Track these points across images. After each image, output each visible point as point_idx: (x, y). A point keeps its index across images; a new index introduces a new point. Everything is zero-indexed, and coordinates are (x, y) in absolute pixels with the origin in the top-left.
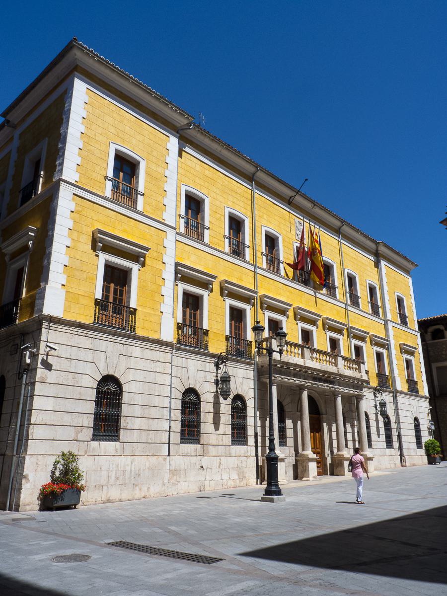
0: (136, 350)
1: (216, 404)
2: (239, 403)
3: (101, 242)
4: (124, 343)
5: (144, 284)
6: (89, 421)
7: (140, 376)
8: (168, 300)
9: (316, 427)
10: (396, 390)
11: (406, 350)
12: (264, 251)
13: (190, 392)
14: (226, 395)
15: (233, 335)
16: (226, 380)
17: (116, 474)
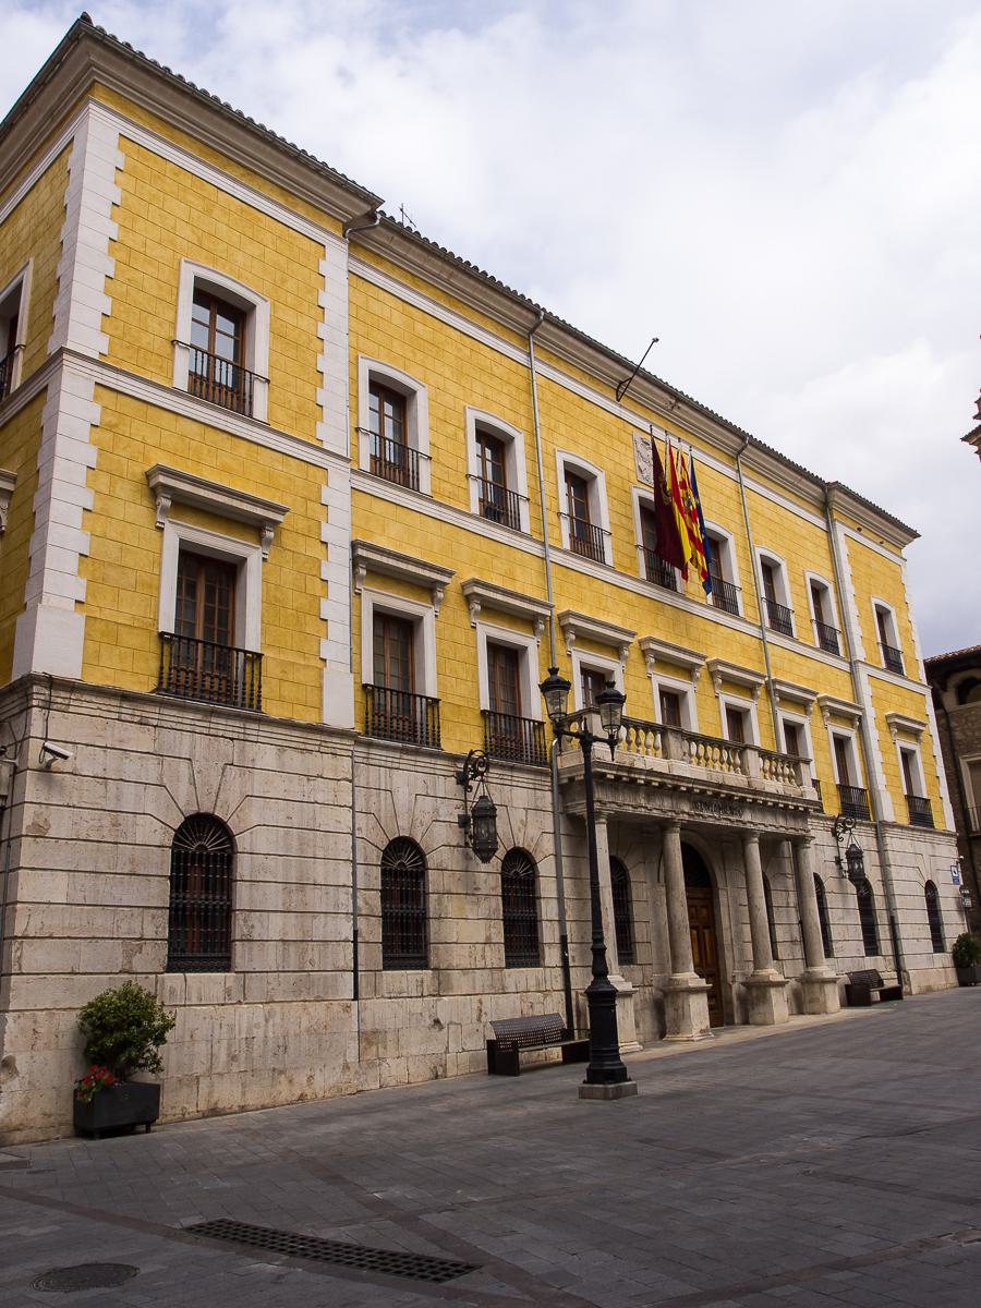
5: (279, 595)
8: (339, 631)
14: (485, 850)
17: (229, 1047)
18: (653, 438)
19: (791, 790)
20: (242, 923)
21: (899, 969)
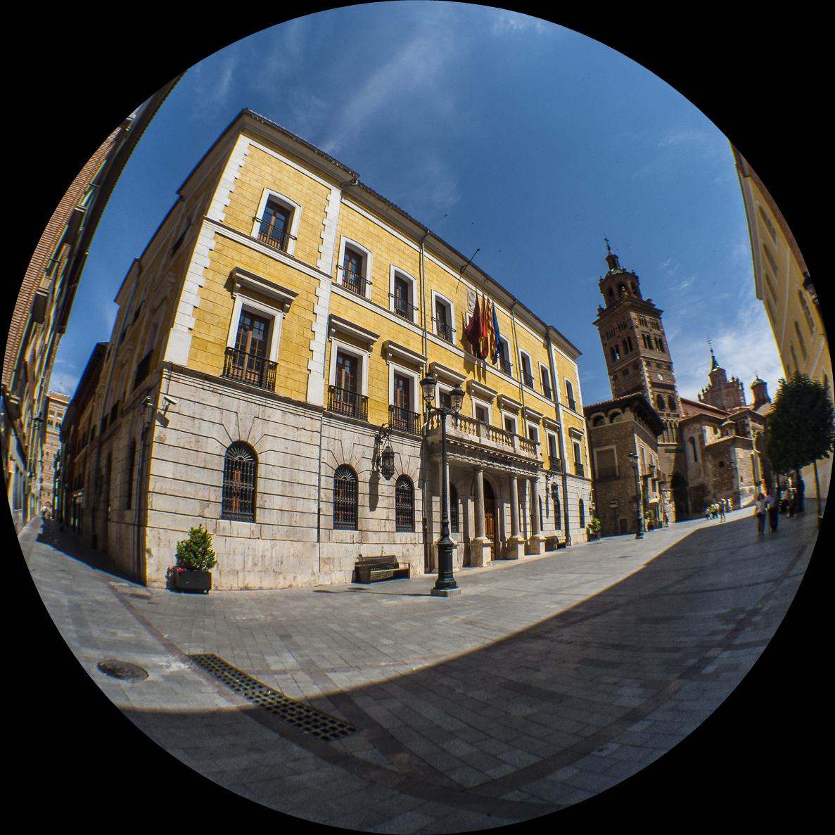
0: (276, 413)
1: (374, 483)
2: (405, 485)
3: (236, 283)
4: (261, 403)
5: (289, 335)
6: (217, 495)
7: (280, 445)
8: (318, 357)
9: (492, 508)
10: (565, 473)
11: (573, 434)
12: (434, 316)
13: (345, 469)
14: (388, 473)
15: (399, 406)
16: (389, 455)
17: (253, 559)
18: (477, 294)
19: (532, 456)
20: (260, 499)
21: (567, 534)
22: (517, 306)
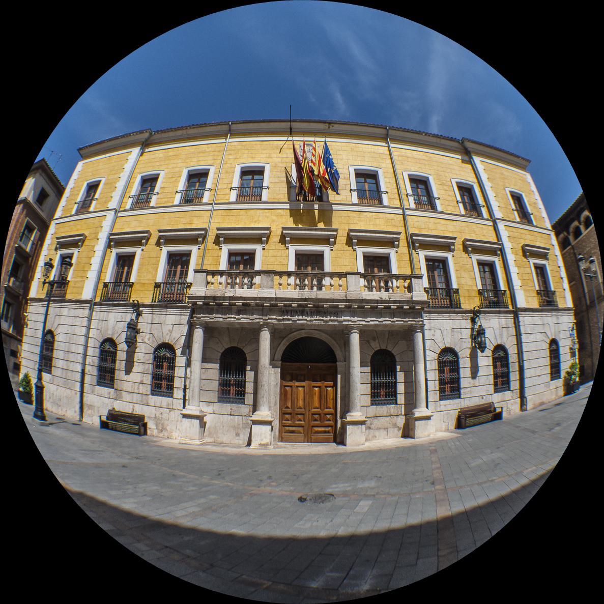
1: (474, 357)
13: (110, 341)
22: (391, 132)
